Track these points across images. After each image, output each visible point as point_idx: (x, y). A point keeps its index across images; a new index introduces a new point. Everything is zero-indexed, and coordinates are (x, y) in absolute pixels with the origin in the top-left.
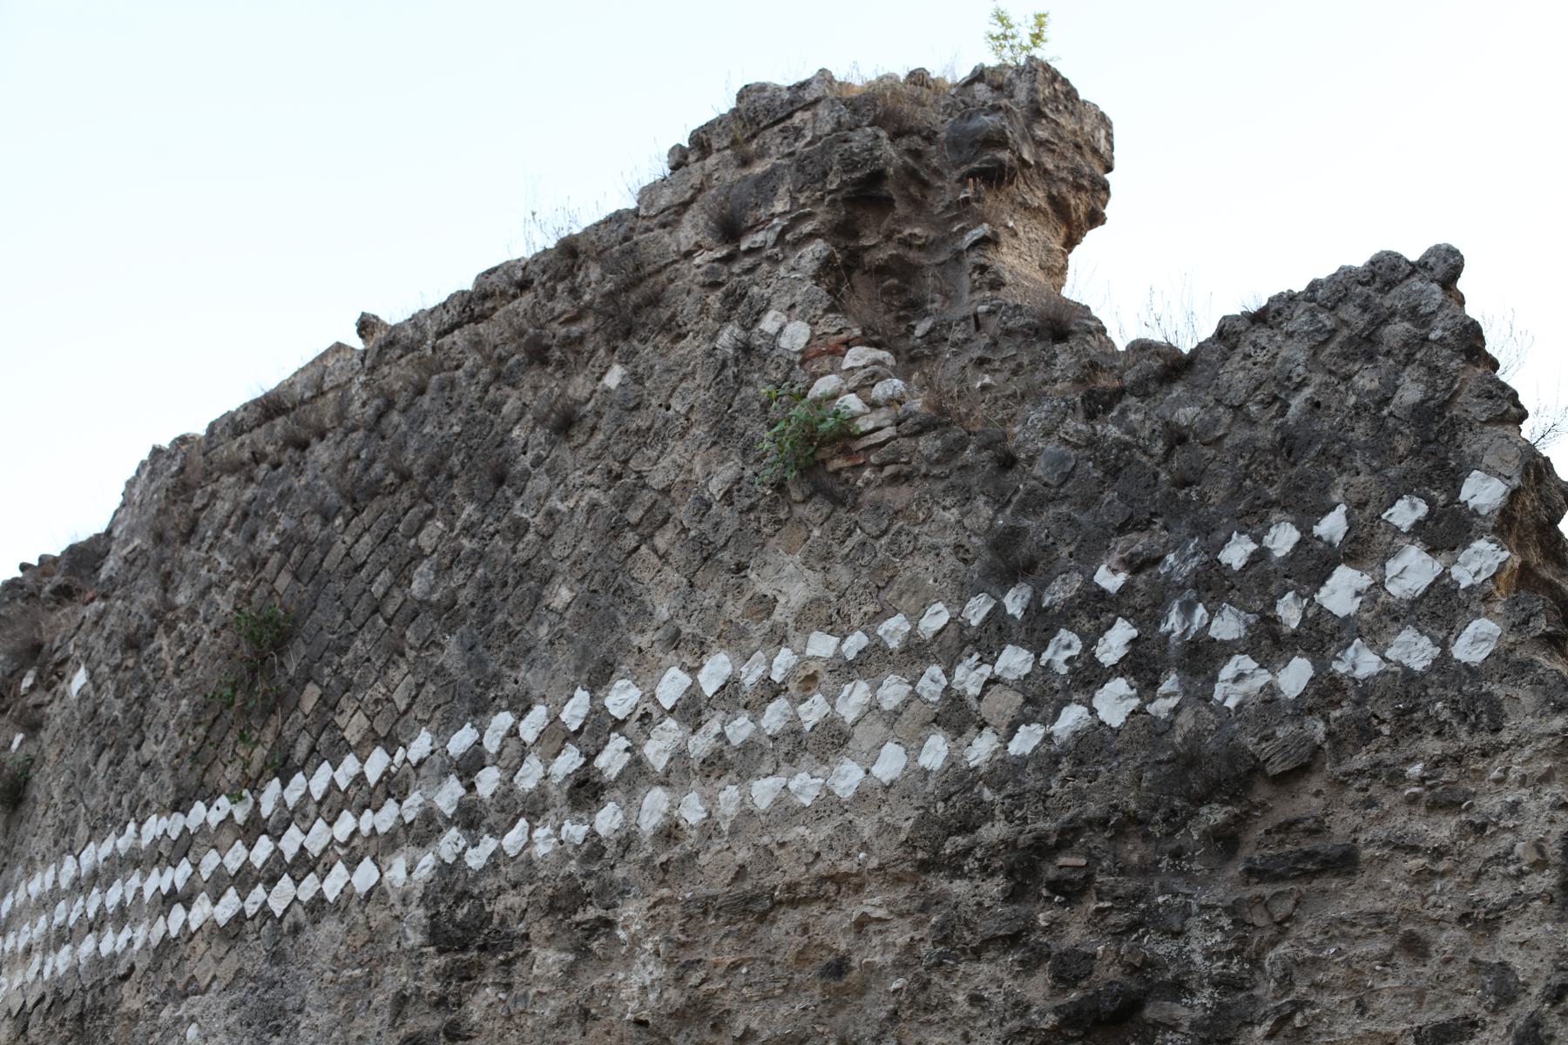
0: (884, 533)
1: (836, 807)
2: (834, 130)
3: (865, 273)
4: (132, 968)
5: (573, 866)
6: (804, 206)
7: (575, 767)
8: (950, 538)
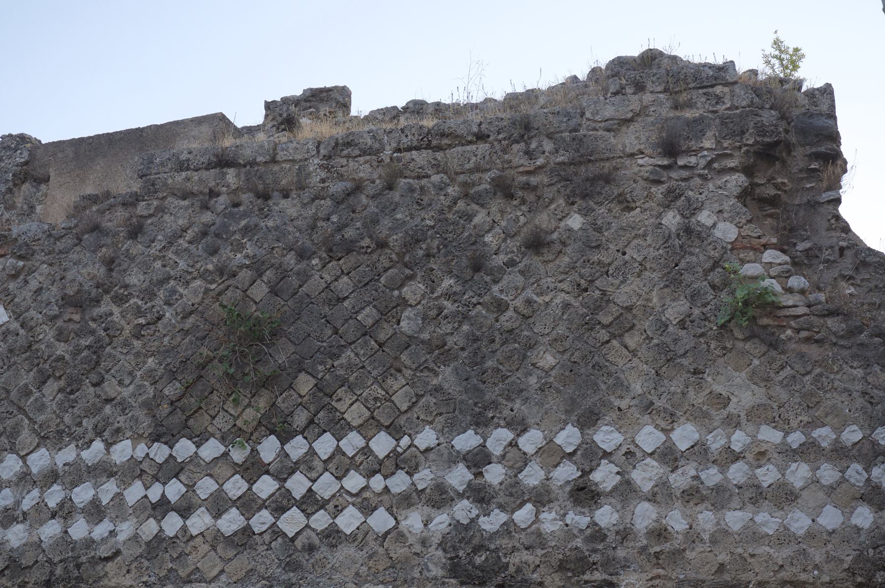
0: (808, 373)
1: (792, 539)
2: (749, 106)
3: (754, 199)
4: (118, 553)
5: (579, 542)
6: (726, 148)
7: (574, 477)
8: (859, 387)
